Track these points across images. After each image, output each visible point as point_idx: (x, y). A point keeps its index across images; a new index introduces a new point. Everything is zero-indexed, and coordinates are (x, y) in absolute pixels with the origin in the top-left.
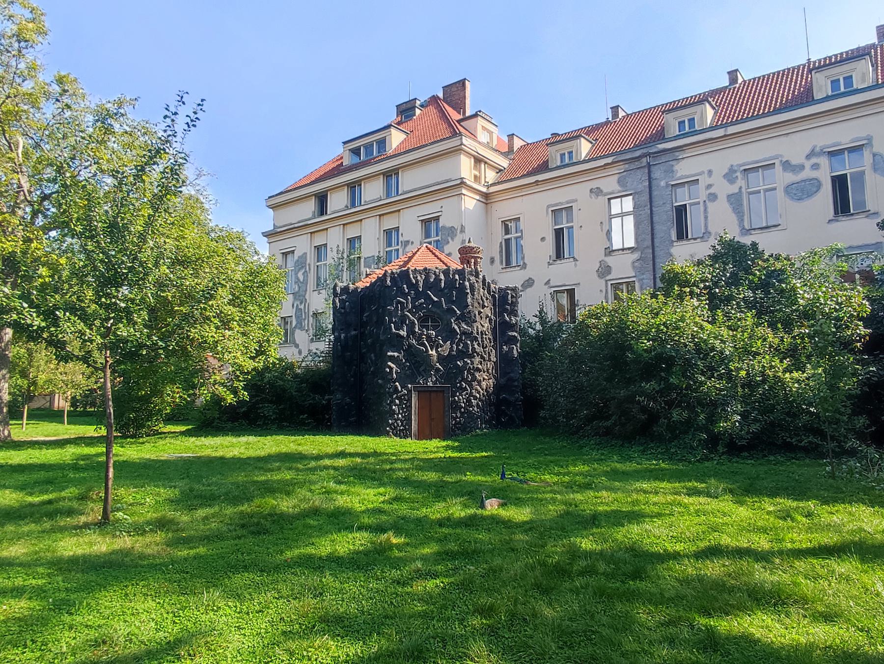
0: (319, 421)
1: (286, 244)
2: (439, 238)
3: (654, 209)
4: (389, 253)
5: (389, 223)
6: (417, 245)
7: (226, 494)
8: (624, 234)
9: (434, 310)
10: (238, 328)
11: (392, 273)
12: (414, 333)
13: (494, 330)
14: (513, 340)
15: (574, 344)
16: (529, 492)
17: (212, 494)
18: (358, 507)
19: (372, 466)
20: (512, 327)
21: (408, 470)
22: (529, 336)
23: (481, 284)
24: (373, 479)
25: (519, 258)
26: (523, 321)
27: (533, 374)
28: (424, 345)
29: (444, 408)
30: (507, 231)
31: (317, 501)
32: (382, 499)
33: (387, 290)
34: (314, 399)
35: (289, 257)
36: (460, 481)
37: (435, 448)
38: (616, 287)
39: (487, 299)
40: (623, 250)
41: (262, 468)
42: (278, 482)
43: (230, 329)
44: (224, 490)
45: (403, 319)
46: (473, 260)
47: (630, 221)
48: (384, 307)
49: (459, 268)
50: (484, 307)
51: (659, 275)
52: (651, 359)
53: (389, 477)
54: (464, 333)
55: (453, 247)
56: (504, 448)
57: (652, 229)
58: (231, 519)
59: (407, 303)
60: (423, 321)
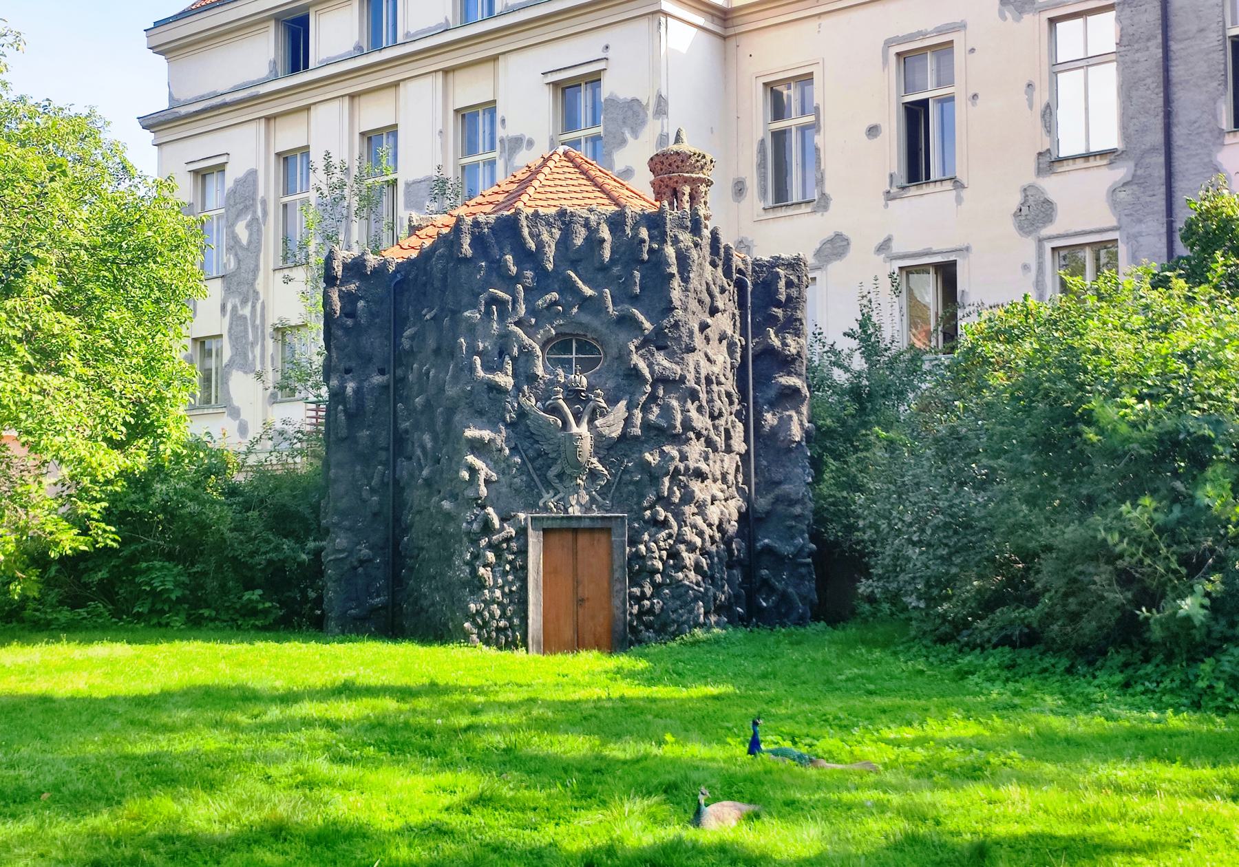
0: (293, 605)
1: (202, 149)
2: (599, 130)
3: (1174, 46)
4: (468, 171)
5: (470, 91)
6: (542, 148)
7: (56, 788)
8: (1093, 111)
9: (585, 318)
10: (80, 369)
11: (476, 224)
12: (532, 378)
13: (740, 373)
14: (792, 395)
15: (947, 408)
16: (819, 786)
17: (20, 788)
18: (383, 820)
19: (422, 720)
20: (787, 363)
21: (513, 729)
22: (833, 386)
23: (707, 250)
24: (426, 751)
25: (811, 182)
26: (817, 347)
27: (841, 486)
28: (555, 410)
29: (612, 571)
30: (779, 109)
31: (283, 805)
32: (446, 800)
33: (463, 269)
34: (277, 549)
35: (212, 181)
36: (645, 757)
37: (591, 675)
38: (1068, 256)
39: (723, 291)
40: (1087, 156)
41: (147, 723)
42: (196, 755)
43: (59, 370)
44: (50, 779)
45: (503, 345)
46: (687, 189)
47: (1106, 79)
48: (455, 313)
49: (651, 210)
50: (713, 311)
51: (1180, 224)
52: (1143, 444)
53: (467, 747)
54: (662, 380)
55: (634, 157)
56: (764, 676)
57: (1168, 101)
58: (66, 848)
59: (515, 301)
60: (558, 346)
